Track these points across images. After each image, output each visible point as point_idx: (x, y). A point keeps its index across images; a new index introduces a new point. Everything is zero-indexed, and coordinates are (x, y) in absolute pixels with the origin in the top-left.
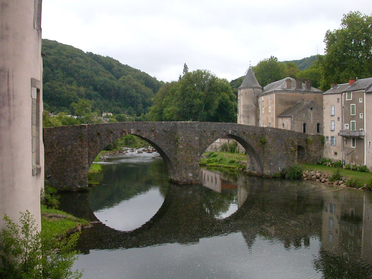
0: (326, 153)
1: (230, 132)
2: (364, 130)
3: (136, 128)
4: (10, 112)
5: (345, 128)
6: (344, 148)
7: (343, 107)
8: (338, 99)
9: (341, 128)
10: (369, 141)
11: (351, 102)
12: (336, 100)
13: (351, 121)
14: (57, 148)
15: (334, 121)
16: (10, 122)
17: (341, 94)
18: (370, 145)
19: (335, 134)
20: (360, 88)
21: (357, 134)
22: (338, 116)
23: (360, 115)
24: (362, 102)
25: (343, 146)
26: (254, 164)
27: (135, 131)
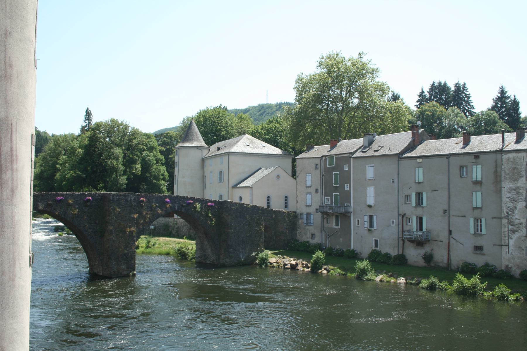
0: (301, 235)
1: (176, 207)
2: (350, 205)
4: (13, 179)
5: (326, 201)
6: (322, 230)
7: (323, 175)
9: (320, 202)
10: (357, 219)
11: (334, 169)
12: (314, 166)
13: (334, 194)
15: (311, 193)
16: (13, 191)
17: (320, 159)
18: (358, 224)
19: (312, 210)
20: (346, 152)
21: (343, 210)
22: (317, 187)
24: (347, 169)
25: (323, 226)
26: (207, 250)
27: (43, 206)
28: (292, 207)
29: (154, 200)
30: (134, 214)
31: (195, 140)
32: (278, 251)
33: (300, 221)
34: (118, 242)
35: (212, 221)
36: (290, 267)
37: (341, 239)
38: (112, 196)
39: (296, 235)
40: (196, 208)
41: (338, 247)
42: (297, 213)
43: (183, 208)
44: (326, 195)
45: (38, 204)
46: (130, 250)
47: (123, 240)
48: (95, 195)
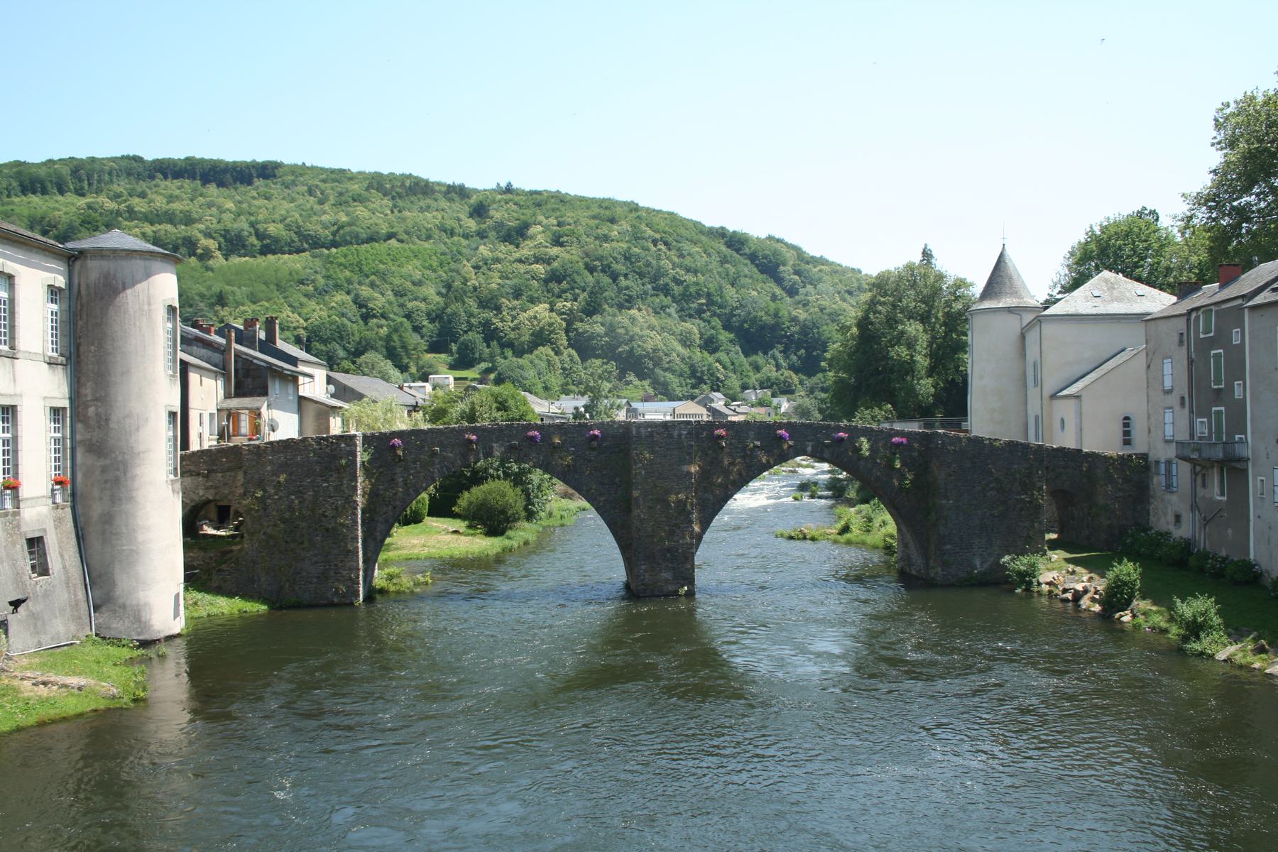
3: (506, 439)
5: (1198, 429)
6: (1194, 507)
8: (1182, 334)
12: (1176, 338)
14: (277, 497)
17: (1185, 318)
23: (1236, 386)
24: (1239, 342)
27: (503, 449)
28: (1139, 446)
29: (751, 434)
30: (690, 463)
31: (1007, 293)
32: (1085, 555)
33: (1155, 480)
34: (651, 524)
35: (903, 477)
36: (1070, 598)
37: (1230, 531)
38: (636, 427)
39: (1149, 515)
40: (861, 450)
41: (1224, 553)
42: (1150, 459)
43: (826, 450)
44: (1200, 415)
45: (492, 447)
46: (681, 541)
47: (664, 519)
48: (612, 426)
